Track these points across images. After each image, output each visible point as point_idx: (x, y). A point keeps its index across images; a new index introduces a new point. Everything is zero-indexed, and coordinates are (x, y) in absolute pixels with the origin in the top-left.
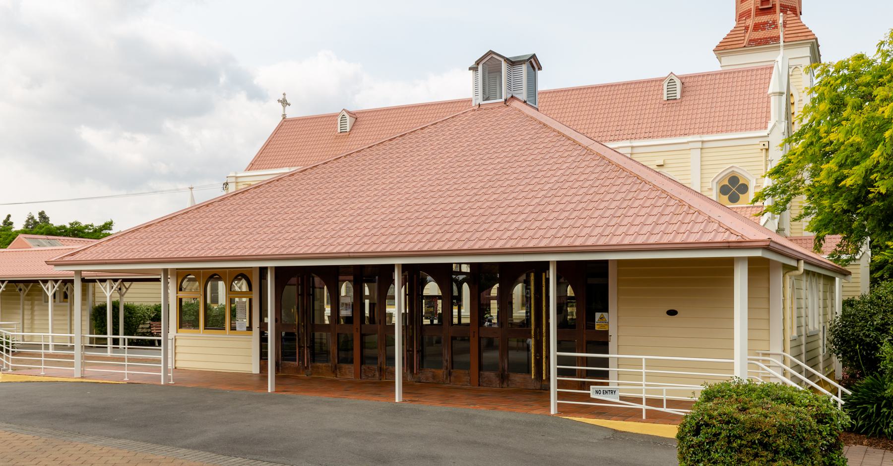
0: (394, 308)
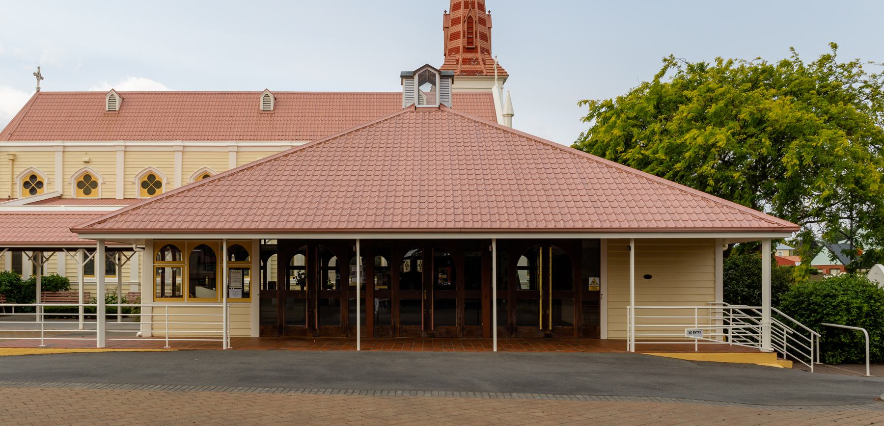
0: (116, 277)
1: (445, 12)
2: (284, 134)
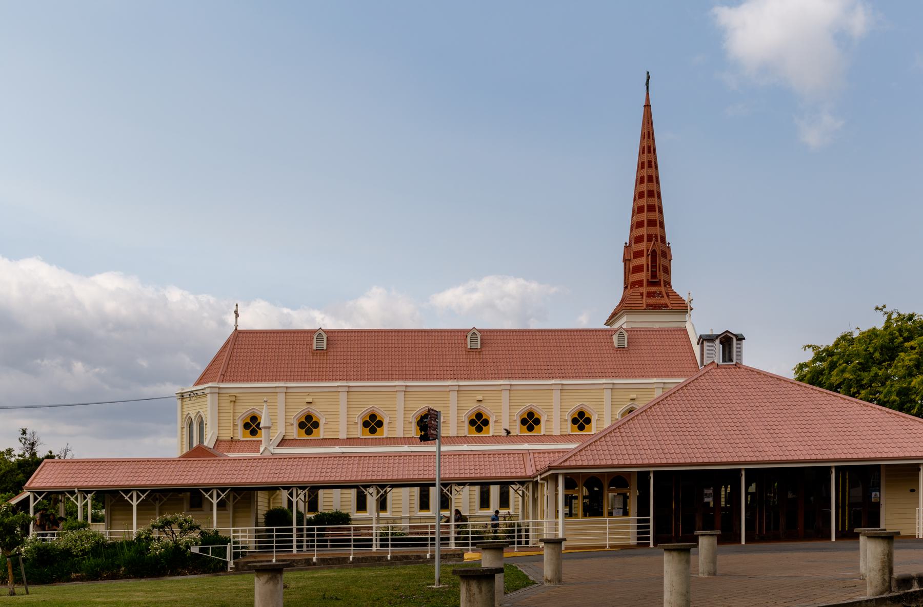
1: (626, 244)
2: (496, 372)
